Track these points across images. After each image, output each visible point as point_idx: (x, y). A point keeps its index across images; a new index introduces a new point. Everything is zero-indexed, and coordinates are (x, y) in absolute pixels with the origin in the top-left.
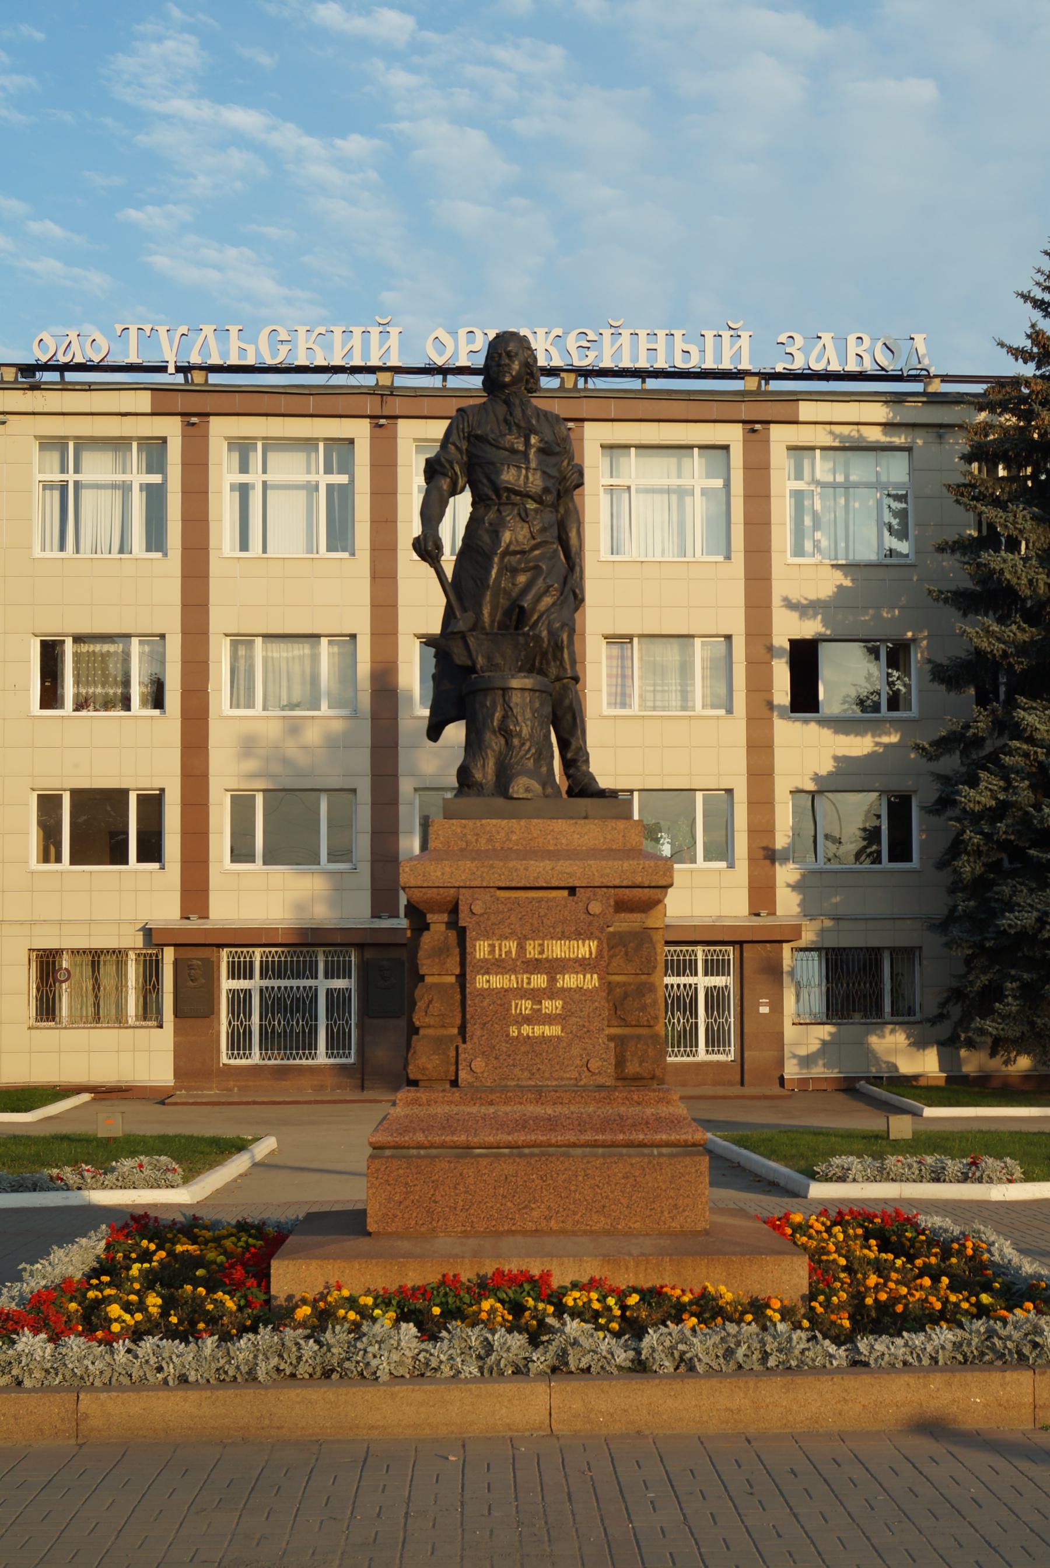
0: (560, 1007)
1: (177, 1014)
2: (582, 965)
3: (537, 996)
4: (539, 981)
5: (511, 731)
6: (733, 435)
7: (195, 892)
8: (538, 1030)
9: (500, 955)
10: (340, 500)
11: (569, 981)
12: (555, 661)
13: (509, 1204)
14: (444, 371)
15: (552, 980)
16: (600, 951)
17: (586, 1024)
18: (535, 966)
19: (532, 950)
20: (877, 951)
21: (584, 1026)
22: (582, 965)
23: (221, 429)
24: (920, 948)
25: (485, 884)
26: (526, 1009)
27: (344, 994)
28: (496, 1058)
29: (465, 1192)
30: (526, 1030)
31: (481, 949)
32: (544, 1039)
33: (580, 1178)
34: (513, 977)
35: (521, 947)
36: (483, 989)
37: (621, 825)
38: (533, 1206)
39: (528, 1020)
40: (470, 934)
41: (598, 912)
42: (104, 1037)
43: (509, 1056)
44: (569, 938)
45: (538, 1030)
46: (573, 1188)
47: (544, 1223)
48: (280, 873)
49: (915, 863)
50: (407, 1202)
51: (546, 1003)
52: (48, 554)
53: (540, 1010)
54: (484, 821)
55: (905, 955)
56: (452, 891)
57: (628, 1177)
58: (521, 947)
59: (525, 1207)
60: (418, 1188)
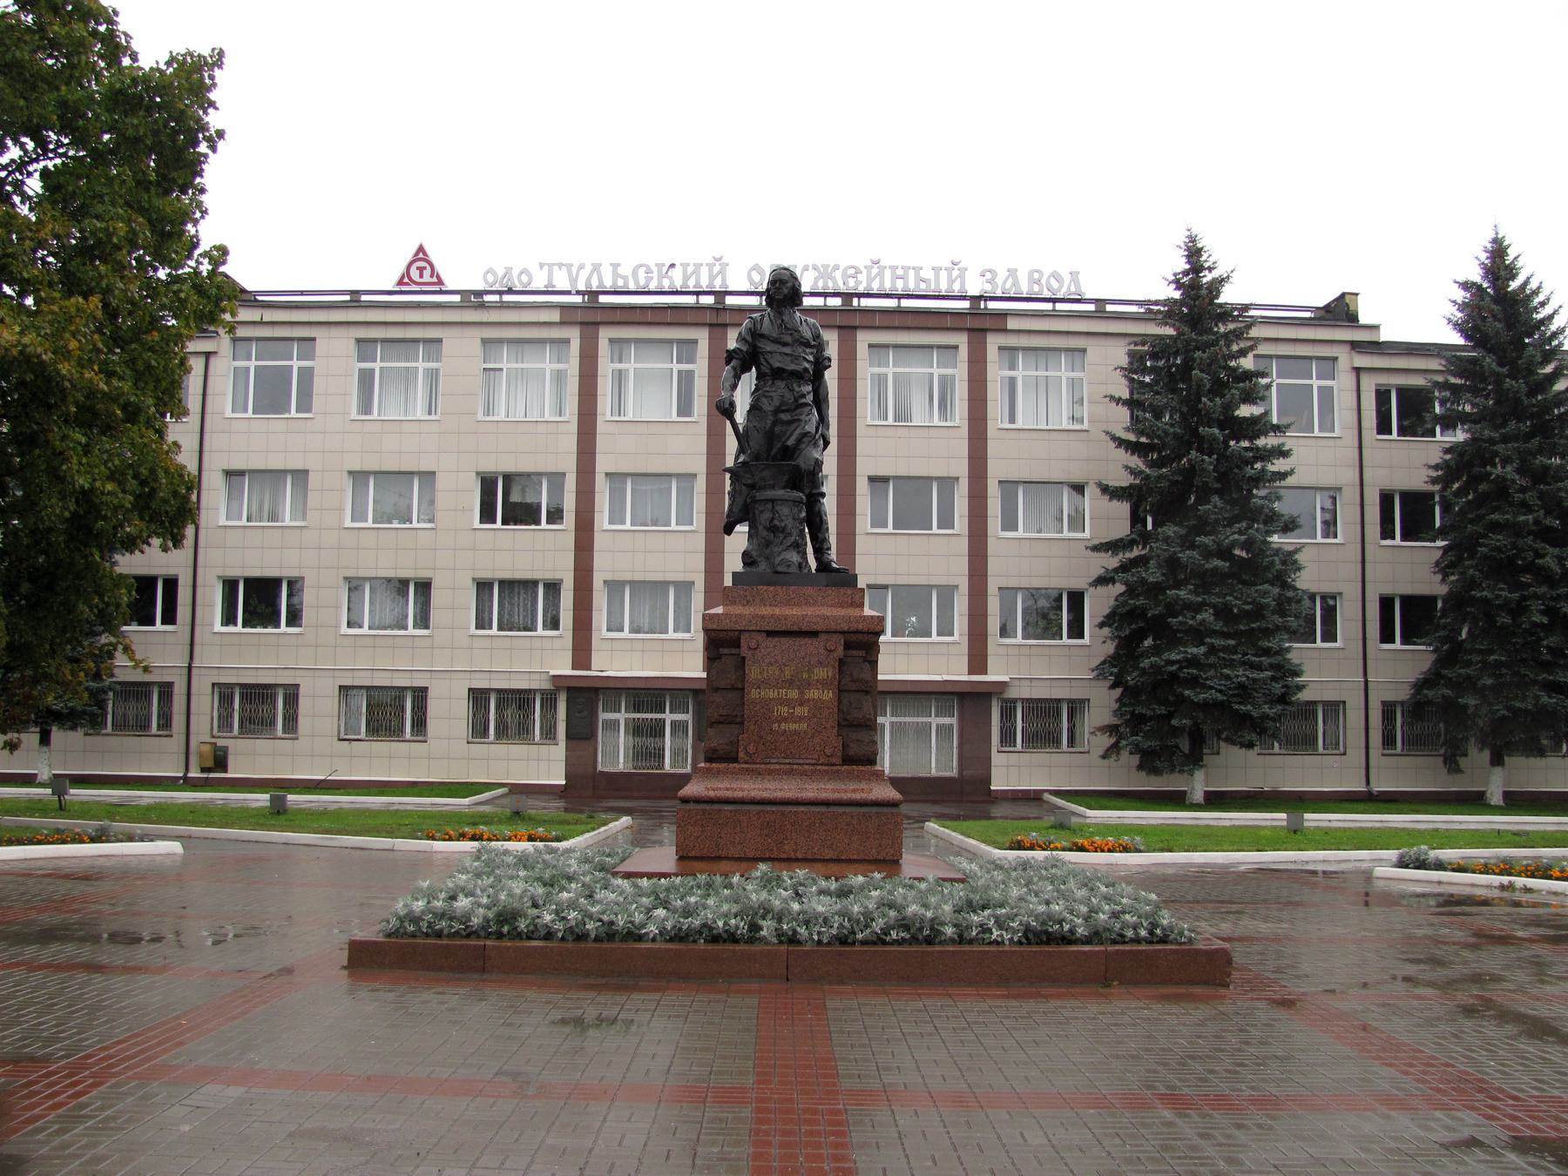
1: (569, 737)
3: (788, 703)
4: (794, 694)
6: (961, 340)
7: (582, 652)
8: (793, 726)
10: (686, 379)
11: (813, 694)
14: (1054, 301)
15: (802, 693)
20: (1059, 701)
22: (823, 684)
27: (684, 724)
30: (783, 726)
31: (753, 672)
32: (796, 733)
37: (849, 591)
39: (785, 720)
42: (518, 750)
45: (793, 726)
49: (1087, 640)
55: (1076, 707)
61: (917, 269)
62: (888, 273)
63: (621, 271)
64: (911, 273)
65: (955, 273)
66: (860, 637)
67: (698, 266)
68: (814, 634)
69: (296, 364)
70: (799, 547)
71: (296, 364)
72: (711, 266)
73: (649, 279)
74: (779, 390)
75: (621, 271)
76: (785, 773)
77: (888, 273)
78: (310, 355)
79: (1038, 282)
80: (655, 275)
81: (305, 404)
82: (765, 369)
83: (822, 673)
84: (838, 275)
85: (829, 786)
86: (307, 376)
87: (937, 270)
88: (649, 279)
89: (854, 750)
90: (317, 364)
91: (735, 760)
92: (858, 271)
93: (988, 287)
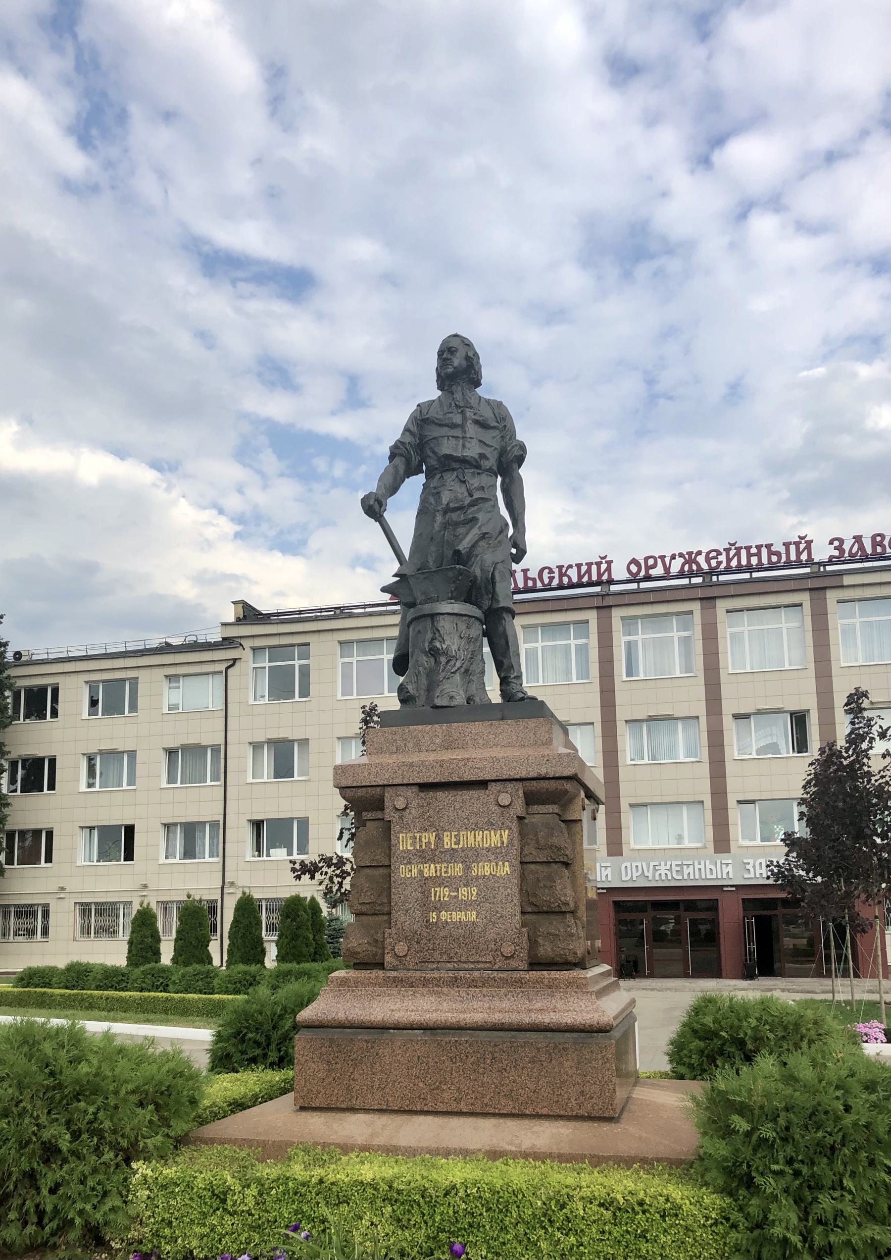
0: (475, 893)
2: (496, 853)
4: (457, 869)
5: (438, 649)
8: (457, 916)
9: (421, 846)
11: (486, 869)
12: (487, 595)
13: (421, 1085)
15: (468, 868)
16: (510, 841)
17: (499, 910)
18: (452, 855)
19: (448, 841)
21: (497, 912)
22: (496, 853)
23: (617, 614)
24: (132, 754)
25: (405, 782)
26: (472, 895)
28: (418, 943)
29: (381, 1071)
31: (404, 842)
33: (489, 1061)
34: (432, 866)
35: (439, 838)
36: (406, 879)
38: (444, 1087)
40: (395, 828)
41: (507, 804)
43: (430, 940)
44: (482, 829)
45: (457, 916)
46: (481, 1070)
47: (454, 1105)
48: (41, 754)
50: (327, 1081)
51: (463, 891)
52: (791, 754)
53: (456, 897)
54: (411, 727)
56: (378, 789)
57: (534, 1062)
58: (439, 838)
59: (437, 1088)
60: (339, 1066)
61: (769, 546)
62: (743, 553)
63: (529, 574)
64: (764, 552)
65: (802, 546)
66: (544, 784)
67: (589, 565)
68: (483, 784)
69: (297, 663)
70: (471, 673)
71: (297, 663)
72: (599, 564)
73: (551, 579)
74: (452, 491)
75: (529, 574)
76: (505, 982)
77: (743, 553)
78: (305, 656)
79: (881, 544)
80: (556, 575)
81: (305, 692)
82: (433, 462)
83: (494, 838)
84: (701, 559)
85: (506, 1004)
86: (305, 672)
87: (787, 545)
88: (551, 579)
89: (546, 950)
90: (312, 662)
91: (381, 965)
92: (719, 553)
93: (836, 553)
